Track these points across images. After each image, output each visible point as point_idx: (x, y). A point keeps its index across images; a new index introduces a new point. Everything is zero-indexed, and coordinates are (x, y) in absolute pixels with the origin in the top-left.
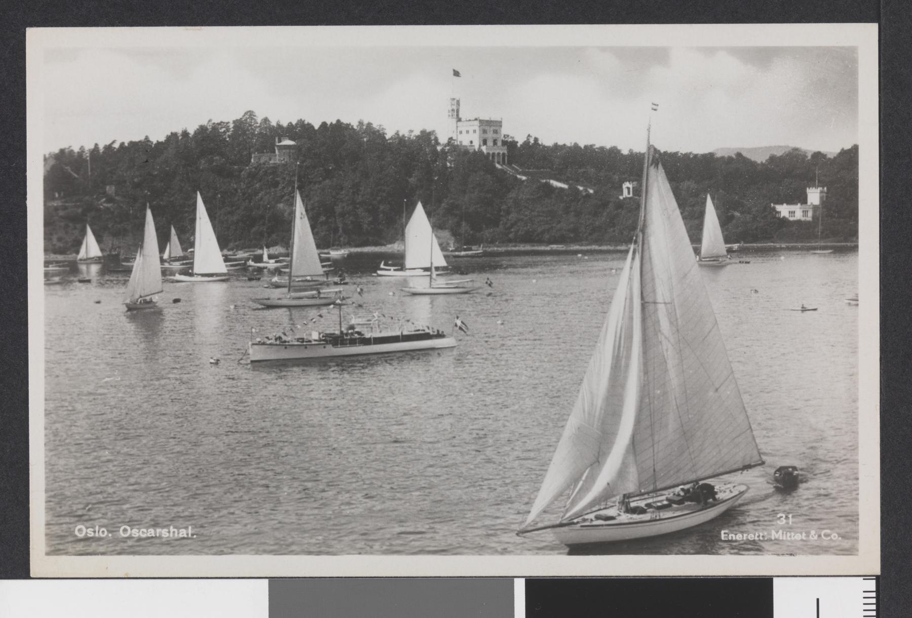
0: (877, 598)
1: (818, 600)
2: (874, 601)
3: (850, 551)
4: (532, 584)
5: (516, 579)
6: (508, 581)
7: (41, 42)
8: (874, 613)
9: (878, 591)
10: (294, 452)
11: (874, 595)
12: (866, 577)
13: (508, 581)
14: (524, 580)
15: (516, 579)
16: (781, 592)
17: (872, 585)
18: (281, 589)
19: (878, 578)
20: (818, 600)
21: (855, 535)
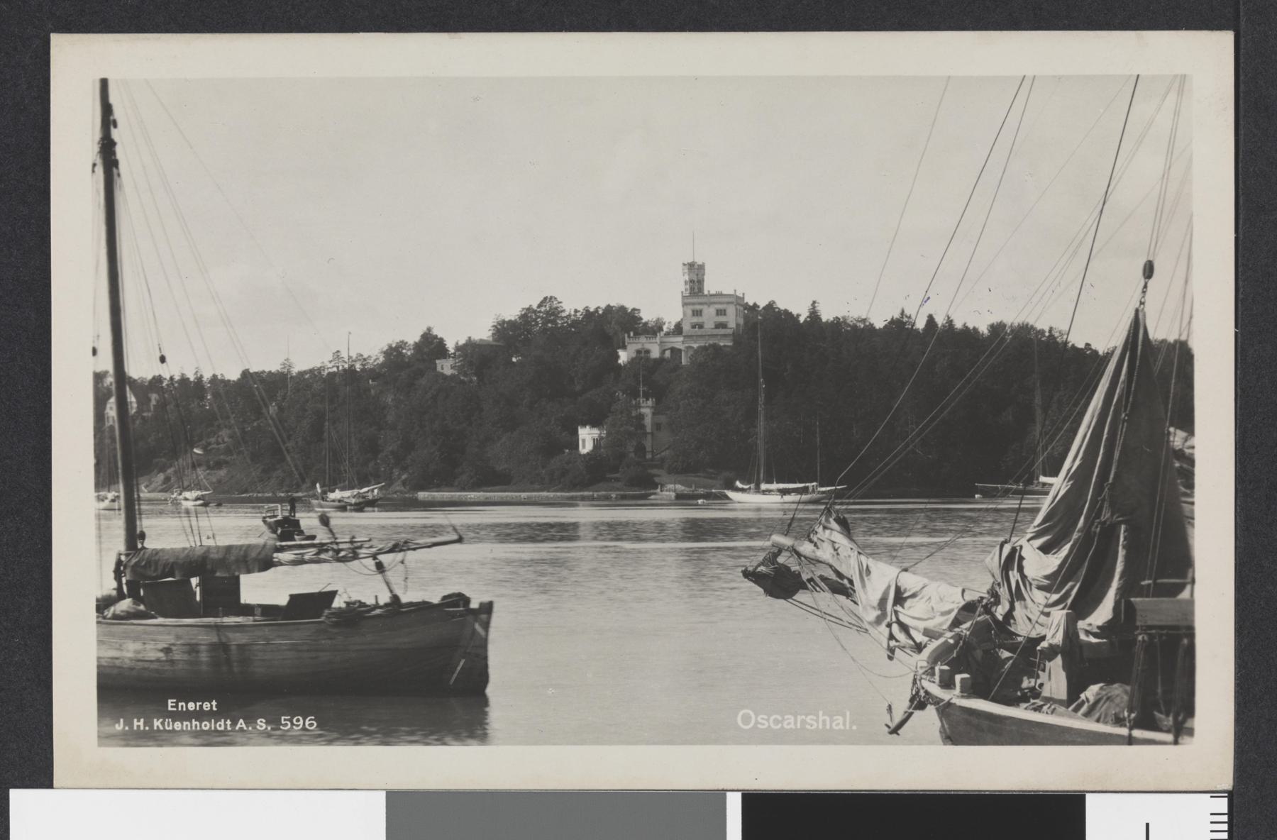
0: (1230, 822)
1: (1147, 825)
2: (1225, 827)
3: (1181, 83)
4: (753, 802)
5: (728, 794)
6: (717, 798)
7: (1202, 61)
8: (1225, 836)
9: (1230, 813)
10: (381, 557)
11: (1225, 818)
12: (1214, 793)
13: (717, 798)
14: (739, 794)
15: (728, 794)
16: (1096, 811)
17: (1222, 805)
18: (405, 809)
19: (1231, 795)
20: (1147, 825)
21: (1190, 500)
